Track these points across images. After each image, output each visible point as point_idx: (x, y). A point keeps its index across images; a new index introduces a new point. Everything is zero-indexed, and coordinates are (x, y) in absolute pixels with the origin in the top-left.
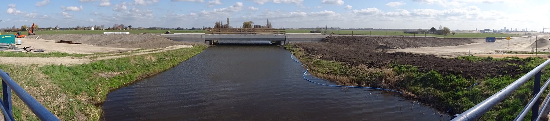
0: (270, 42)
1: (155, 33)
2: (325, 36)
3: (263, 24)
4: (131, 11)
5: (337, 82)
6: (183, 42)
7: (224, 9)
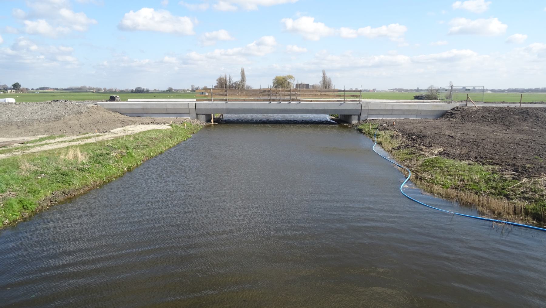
0: (328, 117)
1: (83, 100)
2: (448, 106)
3: (315, 80)
4: (14, 48)
5: (480, 208)
7: (236, 50)
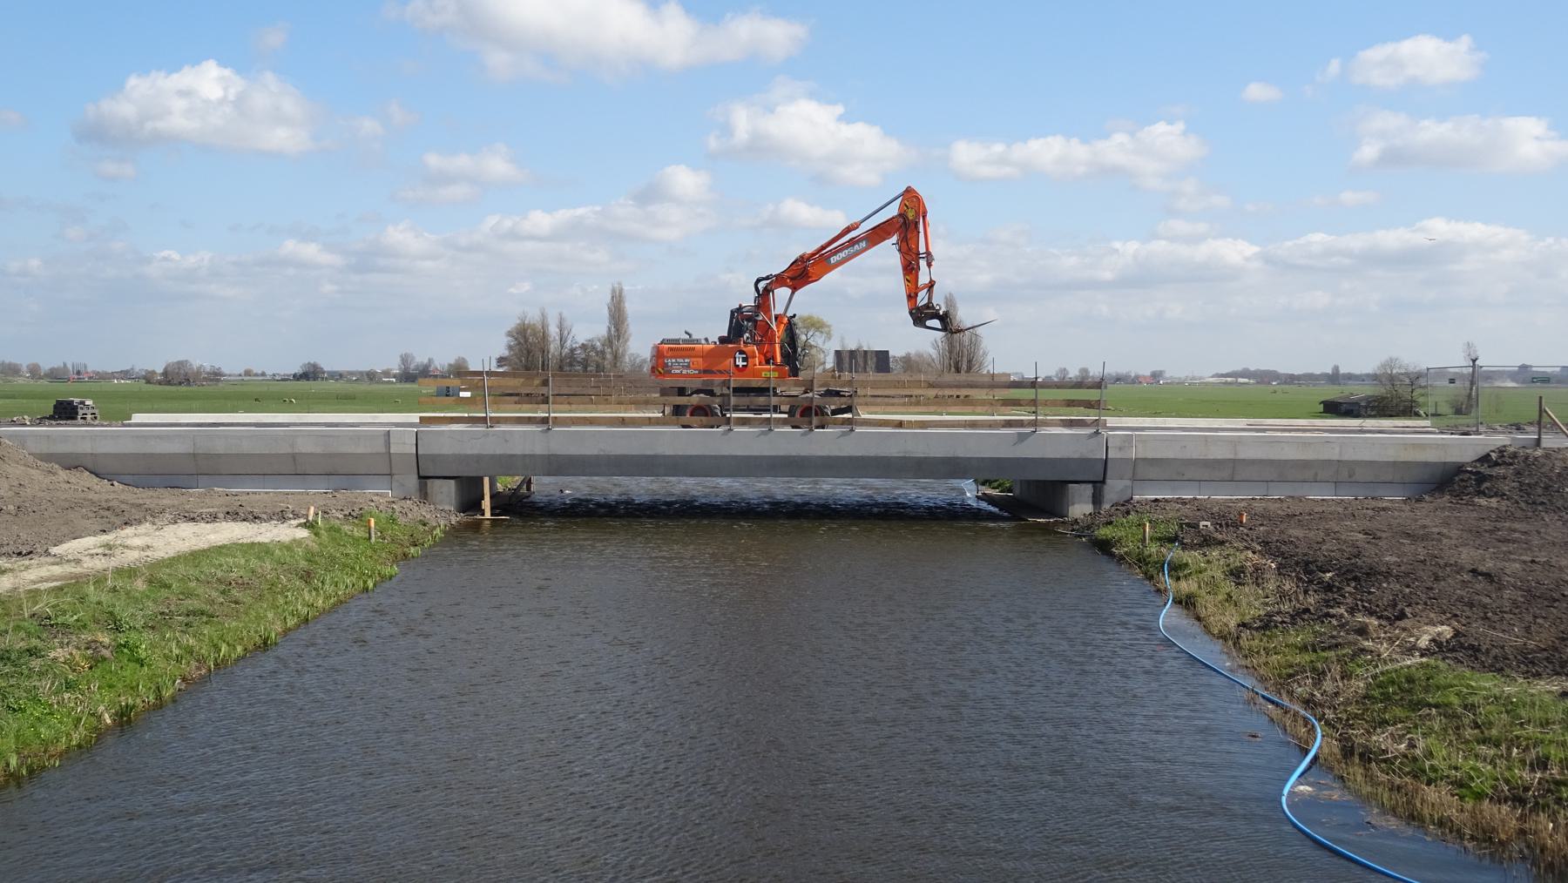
0: (969, 491)
2: (1463, 447)
6: (220, 496)
7: (564, 215)
